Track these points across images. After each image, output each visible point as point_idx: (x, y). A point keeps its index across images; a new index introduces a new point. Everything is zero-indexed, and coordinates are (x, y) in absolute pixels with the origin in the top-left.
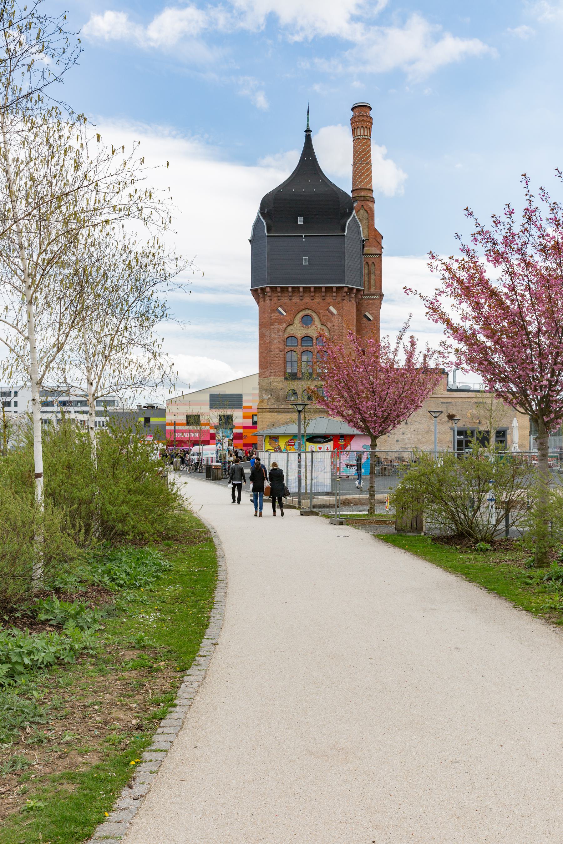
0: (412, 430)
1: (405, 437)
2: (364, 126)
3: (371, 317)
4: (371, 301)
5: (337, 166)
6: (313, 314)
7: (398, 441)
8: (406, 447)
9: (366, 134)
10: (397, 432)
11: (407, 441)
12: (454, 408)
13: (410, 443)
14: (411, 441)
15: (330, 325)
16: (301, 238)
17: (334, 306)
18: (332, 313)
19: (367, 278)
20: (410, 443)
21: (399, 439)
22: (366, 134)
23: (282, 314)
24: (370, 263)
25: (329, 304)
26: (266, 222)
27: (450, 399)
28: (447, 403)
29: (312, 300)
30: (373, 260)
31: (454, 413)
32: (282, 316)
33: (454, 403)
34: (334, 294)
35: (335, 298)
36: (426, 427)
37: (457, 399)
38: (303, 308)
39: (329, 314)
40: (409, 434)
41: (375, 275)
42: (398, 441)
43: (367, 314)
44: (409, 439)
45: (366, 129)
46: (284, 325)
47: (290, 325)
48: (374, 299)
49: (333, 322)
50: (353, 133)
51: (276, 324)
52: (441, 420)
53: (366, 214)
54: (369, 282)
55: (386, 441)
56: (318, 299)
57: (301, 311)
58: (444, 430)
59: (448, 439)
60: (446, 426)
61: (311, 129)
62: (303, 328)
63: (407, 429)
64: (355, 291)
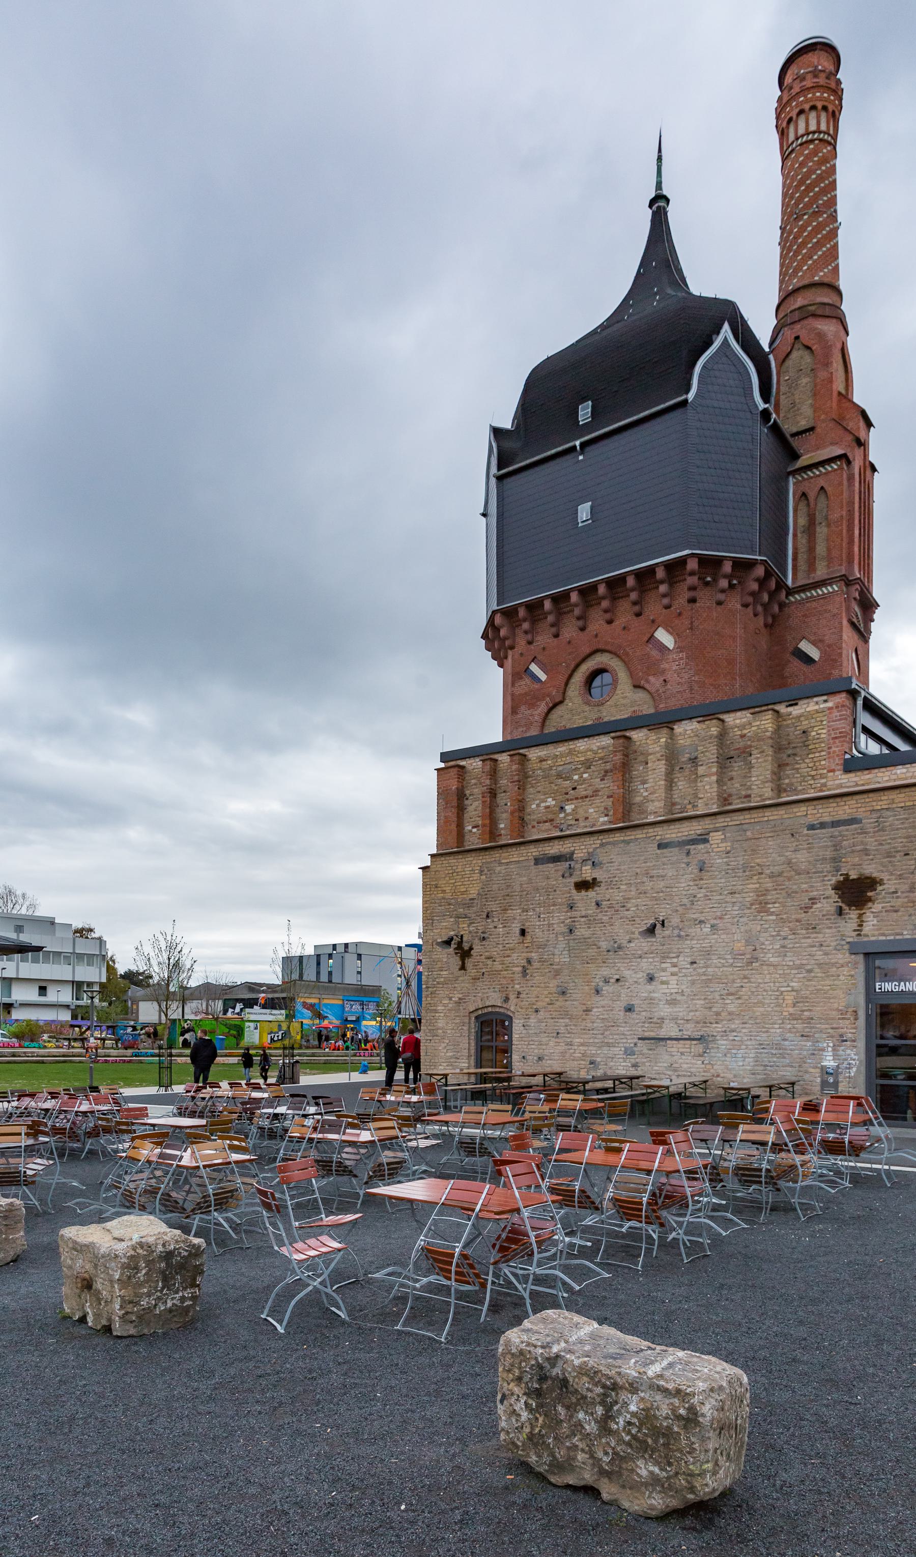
0: (684, 961)
1: (659, 991)
2: (819, 105)
3: (814, 653)
4: (814, 604)
5: (735, 261)
6: (614, 663)
7: (629, 1009)
8: (663, 1033)
9: (823, 127)
10: (627, 973)
11: (665, 1011)
12: (871, 842)
13: (675, 1019)
14: (680, 1011)
15: (655, 682)
16: (573, 455)
17: (670, 630)
18: (662, 648)
19: (803, 540)
20: (675, 1019)
21: (635, 1002)
22: (823, 127)
23: (539, 680)
24: (812, 495)
25: (654, 624)
26: (498, 447)
27: (852, 801)
28: (835, 824)
29: (610, 622)
30: (822, 482)
31: (870, 869)
32: (537, 686)
33: (869, 822)
34: (663, 588)
35: (666, 601)
36: (740, 946)
37: (886, 797)
38: (588, 651)
39: (655, 653)
40: (673, 980)
41: (828, 526)
42: (629, 1009)
43: (805, 646)
44: (672, 1002)
45: (823, 116)
46: (543, 707)
47: (555, 705)
48: (824, 597)
49: (663, 672)
50: (782, 133)
51: (523, 708)
52: (806, 909)
53: (808, 358)
54: (811, 549)
55: (588, 1011)
56: (625, 612)
57: (584, 660)
58: (819, 955)
59: (841, 1001)
60: (828, 935)
61: (665, 192)
62: (587, 708)
63: (664, 957)
64: (727, 567)
